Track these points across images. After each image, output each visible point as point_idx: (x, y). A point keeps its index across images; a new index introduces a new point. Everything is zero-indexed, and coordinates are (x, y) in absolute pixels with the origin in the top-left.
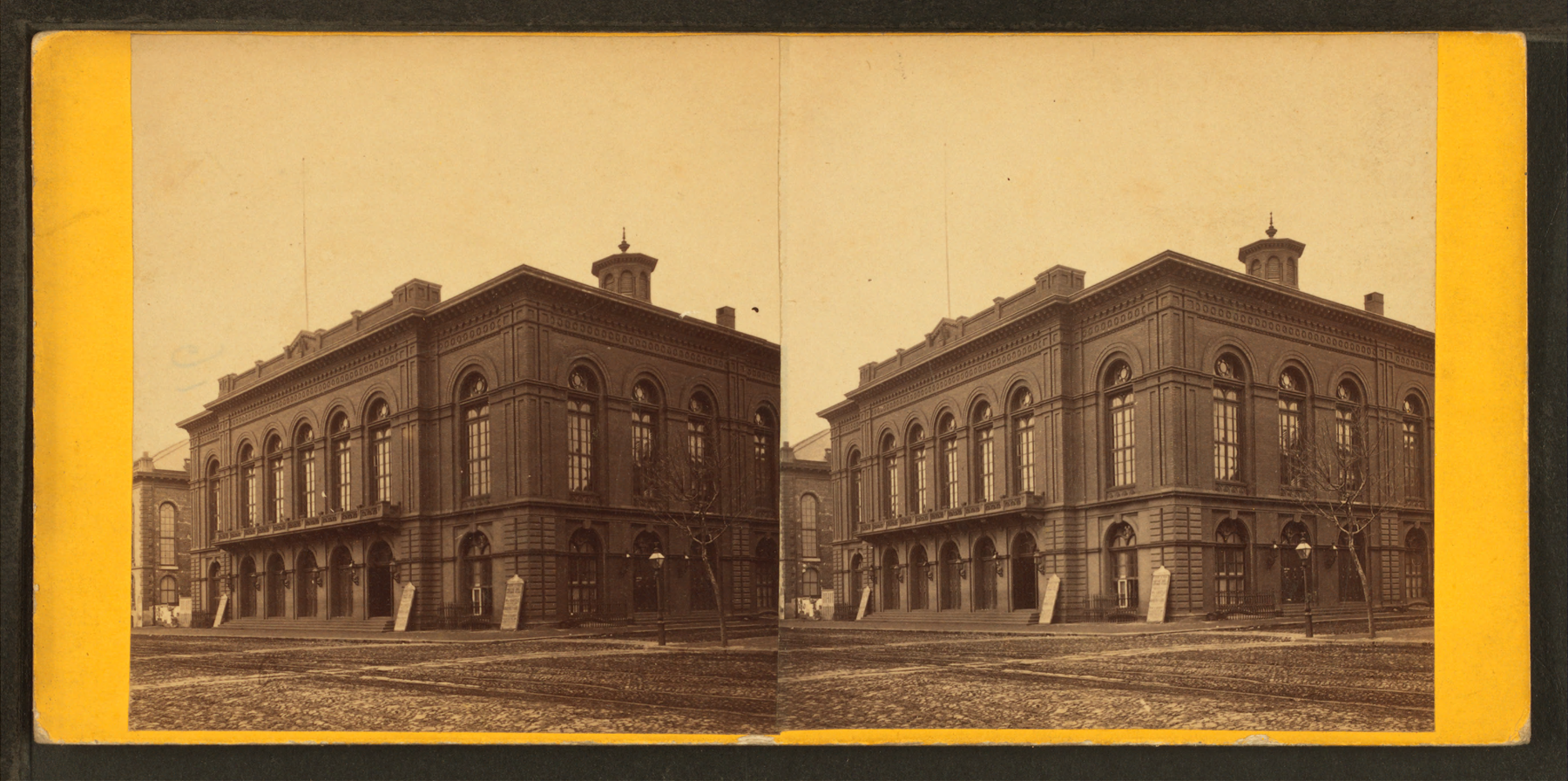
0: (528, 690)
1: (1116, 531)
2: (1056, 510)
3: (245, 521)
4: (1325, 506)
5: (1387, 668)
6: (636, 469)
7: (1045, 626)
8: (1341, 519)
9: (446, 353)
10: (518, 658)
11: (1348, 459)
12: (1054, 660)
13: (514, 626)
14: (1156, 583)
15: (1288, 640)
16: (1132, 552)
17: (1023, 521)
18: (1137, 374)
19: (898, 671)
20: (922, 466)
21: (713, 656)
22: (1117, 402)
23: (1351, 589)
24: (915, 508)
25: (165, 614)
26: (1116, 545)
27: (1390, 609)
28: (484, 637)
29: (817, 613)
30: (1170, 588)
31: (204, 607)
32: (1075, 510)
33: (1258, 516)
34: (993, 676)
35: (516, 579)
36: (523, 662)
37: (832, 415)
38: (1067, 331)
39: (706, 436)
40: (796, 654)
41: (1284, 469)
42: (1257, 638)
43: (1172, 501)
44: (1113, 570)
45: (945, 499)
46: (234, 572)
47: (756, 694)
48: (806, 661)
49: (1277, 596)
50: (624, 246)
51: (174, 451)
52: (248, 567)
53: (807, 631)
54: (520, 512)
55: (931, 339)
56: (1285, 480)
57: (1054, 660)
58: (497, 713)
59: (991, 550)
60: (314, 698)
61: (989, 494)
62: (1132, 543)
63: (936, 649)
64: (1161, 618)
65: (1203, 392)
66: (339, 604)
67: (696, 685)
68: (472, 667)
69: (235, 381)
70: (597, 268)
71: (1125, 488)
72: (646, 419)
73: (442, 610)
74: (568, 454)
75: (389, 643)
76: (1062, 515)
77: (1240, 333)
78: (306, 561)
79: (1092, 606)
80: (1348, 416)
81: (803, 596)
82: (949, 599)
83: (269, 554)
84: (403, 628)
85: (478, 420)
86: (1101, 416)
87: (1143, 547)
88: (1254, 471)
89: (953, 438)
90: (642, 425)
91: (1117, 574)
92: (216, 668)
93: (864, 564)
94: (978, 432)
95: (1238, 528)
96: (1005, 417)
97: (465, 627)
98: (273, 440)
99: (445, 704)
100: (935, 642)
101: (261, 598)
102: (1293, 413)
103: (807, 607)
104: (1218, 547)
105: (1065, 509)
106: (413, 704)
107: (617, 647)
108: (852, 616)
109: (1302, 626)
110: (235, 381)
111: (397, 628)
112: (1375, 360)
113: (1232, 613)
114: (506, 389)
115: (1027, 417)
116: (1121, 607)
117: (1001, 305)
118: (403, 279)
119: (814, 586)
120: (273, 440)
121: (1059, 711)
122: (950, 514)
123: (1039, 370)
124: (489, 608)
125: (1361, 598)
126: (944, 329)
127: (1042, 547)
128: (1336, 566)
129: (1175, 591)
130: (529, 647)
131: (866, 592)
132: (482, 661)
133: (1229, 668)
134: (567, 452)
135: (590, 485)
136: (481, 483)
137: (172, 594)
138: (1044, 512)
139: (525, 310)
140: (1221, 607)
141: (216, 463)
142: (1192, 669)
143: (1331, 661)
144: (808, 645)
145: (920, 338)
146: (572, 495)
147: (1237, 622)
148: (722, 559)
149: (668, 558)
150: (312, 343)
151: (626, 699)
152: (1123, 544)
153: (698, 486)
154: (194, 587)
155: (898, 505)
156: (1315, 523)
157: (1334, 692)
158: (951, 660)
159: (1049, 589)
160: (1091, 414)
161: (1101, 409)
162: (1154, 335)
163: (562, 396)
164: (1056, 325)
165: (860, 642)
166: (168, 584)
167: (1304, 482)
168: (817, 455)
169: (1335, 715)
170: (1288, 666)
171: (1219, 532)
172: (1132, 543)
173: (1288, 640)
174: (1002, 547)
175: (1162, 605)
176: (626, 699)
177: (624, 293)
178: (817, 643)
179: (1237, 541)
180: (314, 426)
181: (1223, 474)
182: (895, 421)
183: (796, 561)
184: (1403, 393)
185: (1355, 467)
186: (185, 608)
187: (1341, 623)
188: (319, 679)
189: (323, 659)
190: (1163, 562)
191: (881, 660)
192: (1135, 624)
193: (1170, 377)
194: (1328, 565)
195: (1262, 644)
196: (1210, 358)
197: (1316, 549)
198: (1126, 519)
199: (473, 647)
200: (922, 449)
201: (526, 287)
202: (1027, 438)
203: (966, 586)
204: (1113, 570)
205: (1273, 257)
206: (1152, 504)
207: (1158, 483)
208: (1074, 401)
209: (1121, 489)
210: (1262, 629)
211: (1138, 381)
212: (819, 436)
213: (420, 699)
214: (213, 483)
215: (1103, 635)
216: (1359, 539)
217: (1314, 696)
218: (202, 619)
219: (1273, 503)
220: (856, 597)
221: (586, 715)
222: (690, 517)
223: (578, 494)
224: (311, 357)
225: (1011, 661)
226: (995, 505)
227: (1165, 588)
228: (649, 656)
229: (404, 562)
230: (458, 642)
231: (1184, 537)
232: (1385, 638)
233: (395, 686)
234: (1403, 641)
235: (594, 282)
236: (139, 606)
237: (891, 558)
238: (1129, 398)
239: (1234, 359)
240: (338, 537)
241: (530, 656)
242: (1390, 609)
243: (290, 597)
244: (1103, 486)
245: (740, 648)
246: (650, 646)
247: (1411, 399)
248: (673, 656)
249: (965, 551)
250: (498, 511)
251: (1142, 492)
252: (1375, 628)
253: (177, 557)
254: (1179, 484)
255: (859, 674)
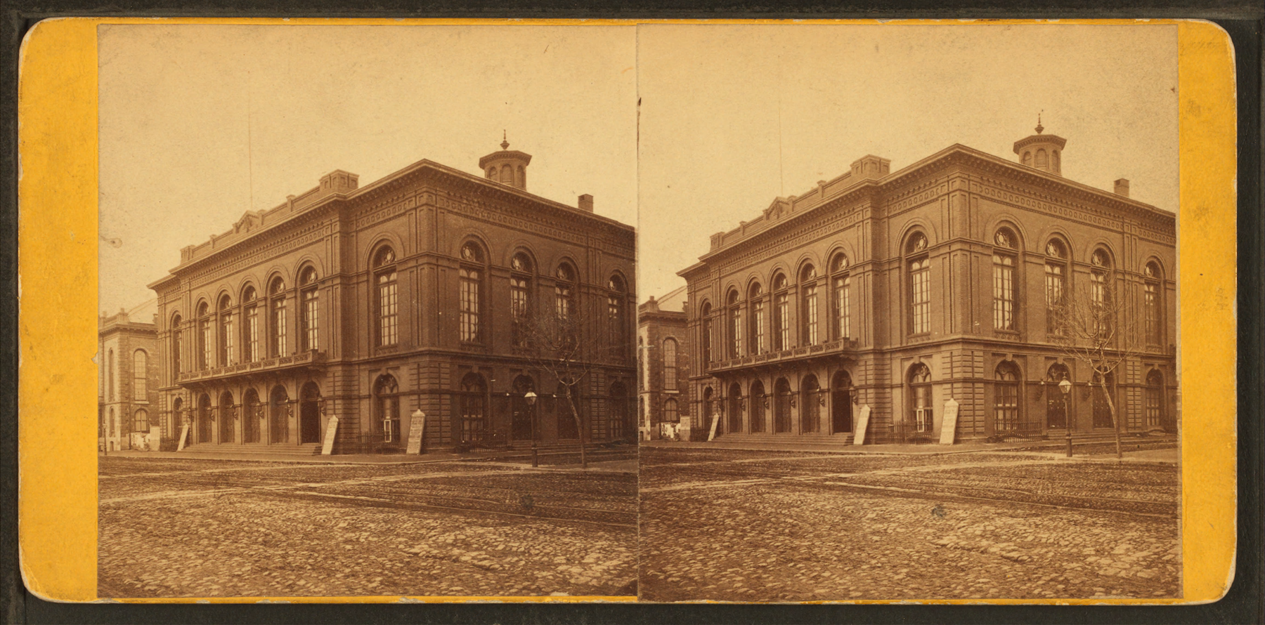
0: (429, 503)
1: (915, 369)
2: (867, 353)
3: (732, 352)
4: (1082, 351)
5: (1132, 482)
6: (1049, 312)
7: (858, 447)
8: (1095, 361)
9: (895, 216)
10: (421, 477)
11: (1100, 313)
12: (868, 475)
13: (417, 451)
14: (947, 413)
15: (518, 469)
16: (928, 387)
17: (839, 363)
18: (932, 243)
19: (741, 482)
20: (760, 316)
21: (576, 476)
22: (384, 279)
23: (568, 428)
24: (755, 350)
25: (138, 440)
26: (915, 381)
27: (1134, 435)
28: (395, 459)
29: (677, 435)
30: (958, 416)
31: (700, 424)
32: (350, 364)
33: (1029, 358)
34: (817, 487)
35: (419, 413)
36: (424, 480)
37: (688, 275)
38: (876, 208)
39: (570, 299)
40: (133, 479)
41: (1049, 320)
42: (1028, 457)
43: (960, 346)
44: (913, 401)
45: (248, 355)
46: (724, 395)
47: (611, 506)
48: (666, 475)
49: (1045, 422)
50: (505, 145)
51: (145, 309)
52: (205, 401)
53: (668, 450)
54: (954, 347)
55: (768, 213)
56: (1050, 330)
57: (868, 475)
58: (404, 522)
59: (818, 385)
60: (258, 509)
61: (814, 339)
62: (928, 380)
63: (771, 465)
64: (951, 441)
65: (986, 258)
66: (278, 433)
67: (561, 499)
68: (385, 484)
69: (194, 251)
70: (483, 163)
71: (922, 335)
72: (522, 284)
73: (359, 437)
74: (460, 312)
75: (318, 464)
76: (872, 356)
77: (1014, 211)
78: (251, 397)
79: (896, 431)
80: (1101, 279)
81: (666, 421)
82: (782, 424)
83: (222, 391)
84: (861, 442)
85: (388, 284)
86: (903, 278)
87: (404, 394)
88: (1025, 322)
89: (785, 294)
90: (518, 288)
91: (383, 416)
92: (181, 484)
93: (184, 406)
94: (805, 289)
95: (1013, 368)
96: (826, 277)
97: (379, 451)
98: (224, 299)
99: (364, 515)
100: (771, 459)
101: (215, 427)
102: (522, 289)
103: (669, 430)
104: (997, 384)
105: (874, 352)
106: (866, 505)
107: (499, 468)
108: (704, 438)
109: (1063, 448)
110: (194, 251)
111: (856, 442)
112: (1123, 233)
113: (474, 447)
114: (410, 259)
115: (313, 289)
116: (918, 432)
117: (293, 201)
118: (330, 169)
119: (674, 413)
120: (224, 299)
121: (870, 516)
122: (783, 355)
123: (853, 238)
124: (397, 436)
125: (1111, 426)
126: (778, 206)
127: (856, 383)
128: (1091, 399)
129: (429, 429)
130: (427, 468)
131: (716, 418)
132: (392, 479)
133: (472, 492)
134: (460, 312)
135: (477, 337)
136: (390, 336)
137: (144, 424)
138: (858, 354)
139: (425, 195)
140: (999, 432)
141: (708, 305)
142: (974, 482)
143: (1087, 478)
144: (666, 461)
145: (229, 227)
146: (463, 345)
147: (1011, 444)
148: (1119, 386)
149: (539, 396)
150: (785, 206)
151: (1038, 502)
152: (388, 391)
153: (564, 338)
154: (161, 418)
155: (211, 359)
156: (1074, 364)
157: (1089, 501)
158: (253, 484)
159: (330, 427)
160: (363, 288)
161: (371, 284)
162: (945, 211)
163: (990, 252)
164: (868, 204)
165: (711, 459)
166: (142, 416)
167: (1065, 332)
168: (675, 306)
169: (1090, 520)
170: (1052, 480)
171: (997, 371)
172: (928, 380)
173: (518, 469)
174: (824, 382)
175: (952, 430)
176: (1038, 502)
177: (504, 182)
178: (676, 460)
179: (1012, 379)
180: (788, 275)
181: (1000, 325)
182: (739, 280)
183: (659, 393)
184: (1145, 261)
185: (1107, 320)
186: (155, 435)
187: (1094, 446)
188: (262, 494)
189: (265, 478)
190: (952, 394)
191: (727, 474)
192: (930, 445)
193: (425, 260)
194: (1085, 398)
195: (1030, 462)
196: (457, 245)
197: (1075, 385)
198: (923, 360)
199: (917, 458)
200: (760, 302)
201: (426, 176)
202: (313, 307)
203: (795, 413)
204: (913, 401)
205: (504, 166)
206: (943, 348)
207: (948, 332)
208: (351, 278)
209: (918, 336)
210: (1032, 450)
211: (933, 249)
212: (680, 290)
213: (342, 510)
214: (707, 321)
215: (905, 454)
216: (1109, 378)
217: (1074, 505)
218: (169, 445)
219: (506, 360)
220: (708, 422)
221: (475, 524)
222: (557, 363)
223: (469, 344)
224: (254, 232)
225: (831, 475)
226: (818, 348)
227: (954, 417)
228: (1058, 466)
229: (861, 387)
230: (372, 464)
231: (970, 375)
232: (1130, 458)
233: (323, 499)
234: (1143, 460)
235: (481, 174)
236: (118, 433)
237: (735, 390)
238: (926, 263)
239: (1009, 233)
240: (276, 378)
241: (430, 475)
242: (1134, 435)
243: (238, 426)
244: (905, 333)
245: (598, 470)
246: (525, 467)
247: (615, 279)
248: (1078, 466)
249: (794, 385)
250: (403, 358)
251: (936, 338)
252: (587, 461)
253: (148, 394)
254: (965, 332)
255: (709, 485)
